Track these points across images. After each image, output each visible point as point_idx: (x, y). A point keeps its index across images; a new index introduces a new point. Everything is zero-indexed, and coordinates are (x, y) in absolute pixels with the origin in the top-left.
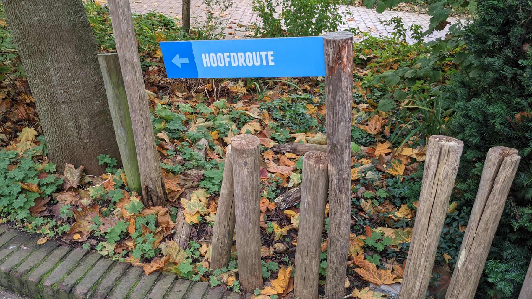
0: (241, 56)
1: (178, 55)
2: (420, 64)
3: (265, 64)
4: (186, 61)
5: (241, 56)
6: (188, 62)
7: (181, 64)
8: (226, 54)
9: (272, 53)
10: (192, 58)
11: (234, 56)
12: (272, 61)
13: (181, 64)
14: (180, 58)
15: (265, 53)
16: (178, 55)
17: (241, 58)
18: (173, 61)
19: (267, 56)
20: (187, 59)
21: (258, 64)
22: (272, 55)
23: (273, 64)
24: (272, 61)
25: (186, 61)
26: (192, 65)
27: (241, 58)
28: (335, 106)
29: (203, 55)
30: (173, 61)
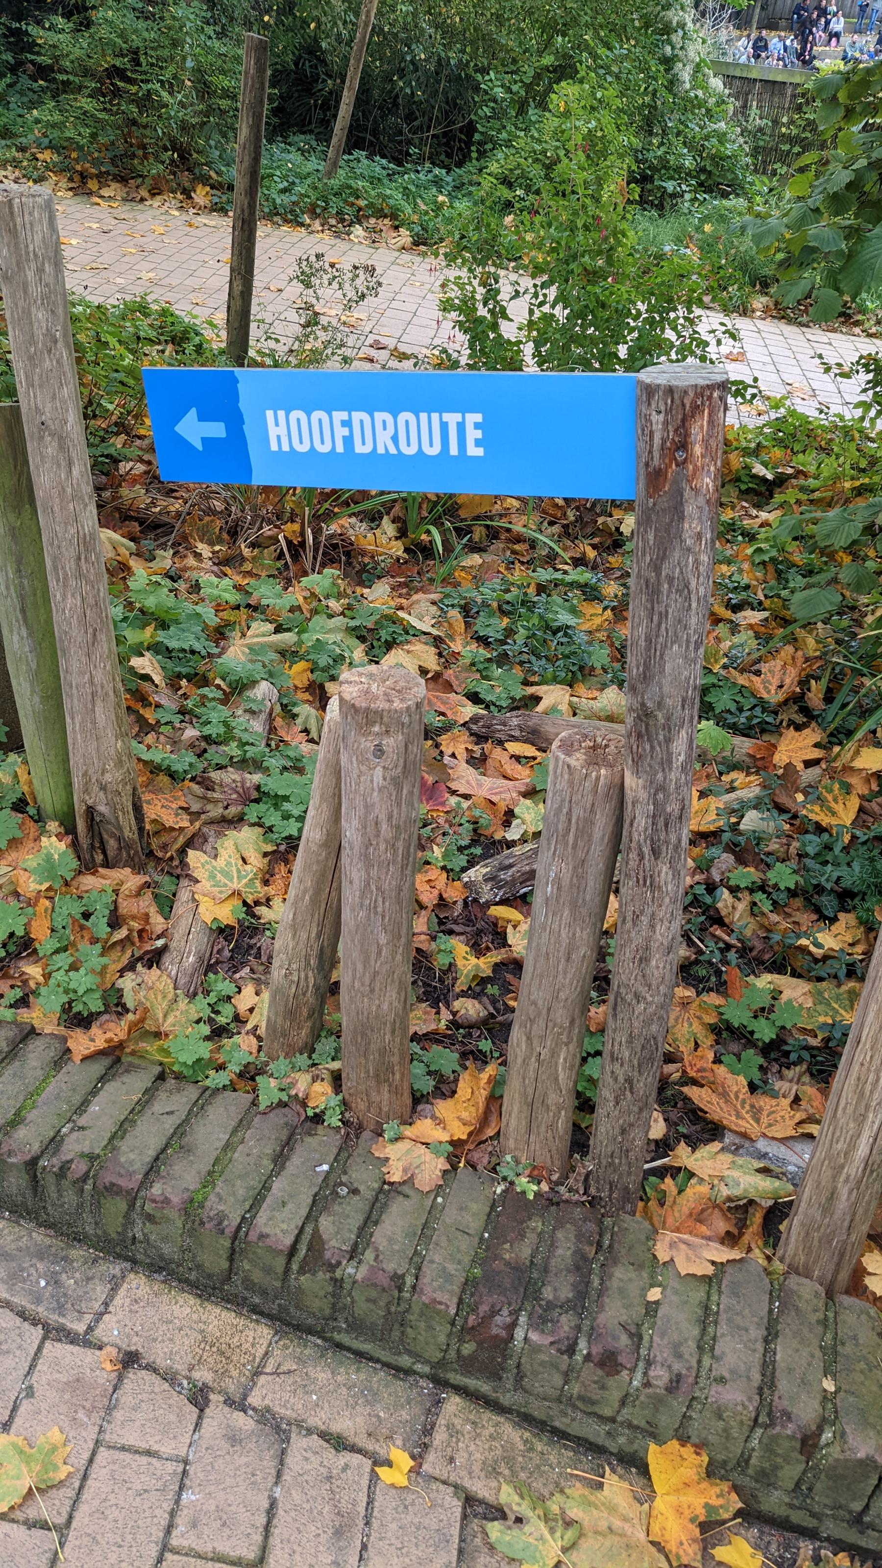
0: (384, 422)
1: (194, 410)
3: (454, 451)
4: (217, 430)
5: (384, 422)
6: (177, 429)
7: (203, 440)
8: (340, 416)
9: (478, 417)
11: (362, 422)
12: (478, 443)
13: (203, 440)
14: (200, 419)
15: (458, 417)
16: (194, 410)
17: (385, 428)
18: (179, 428)
19: (461, 427)
20: (222, 425)
22: (477, 426)
23: (480, 452)
24: (478, 443)
25: (217, 430)
27: (385, 428)
29: (270, 414)
30: (179, 428)
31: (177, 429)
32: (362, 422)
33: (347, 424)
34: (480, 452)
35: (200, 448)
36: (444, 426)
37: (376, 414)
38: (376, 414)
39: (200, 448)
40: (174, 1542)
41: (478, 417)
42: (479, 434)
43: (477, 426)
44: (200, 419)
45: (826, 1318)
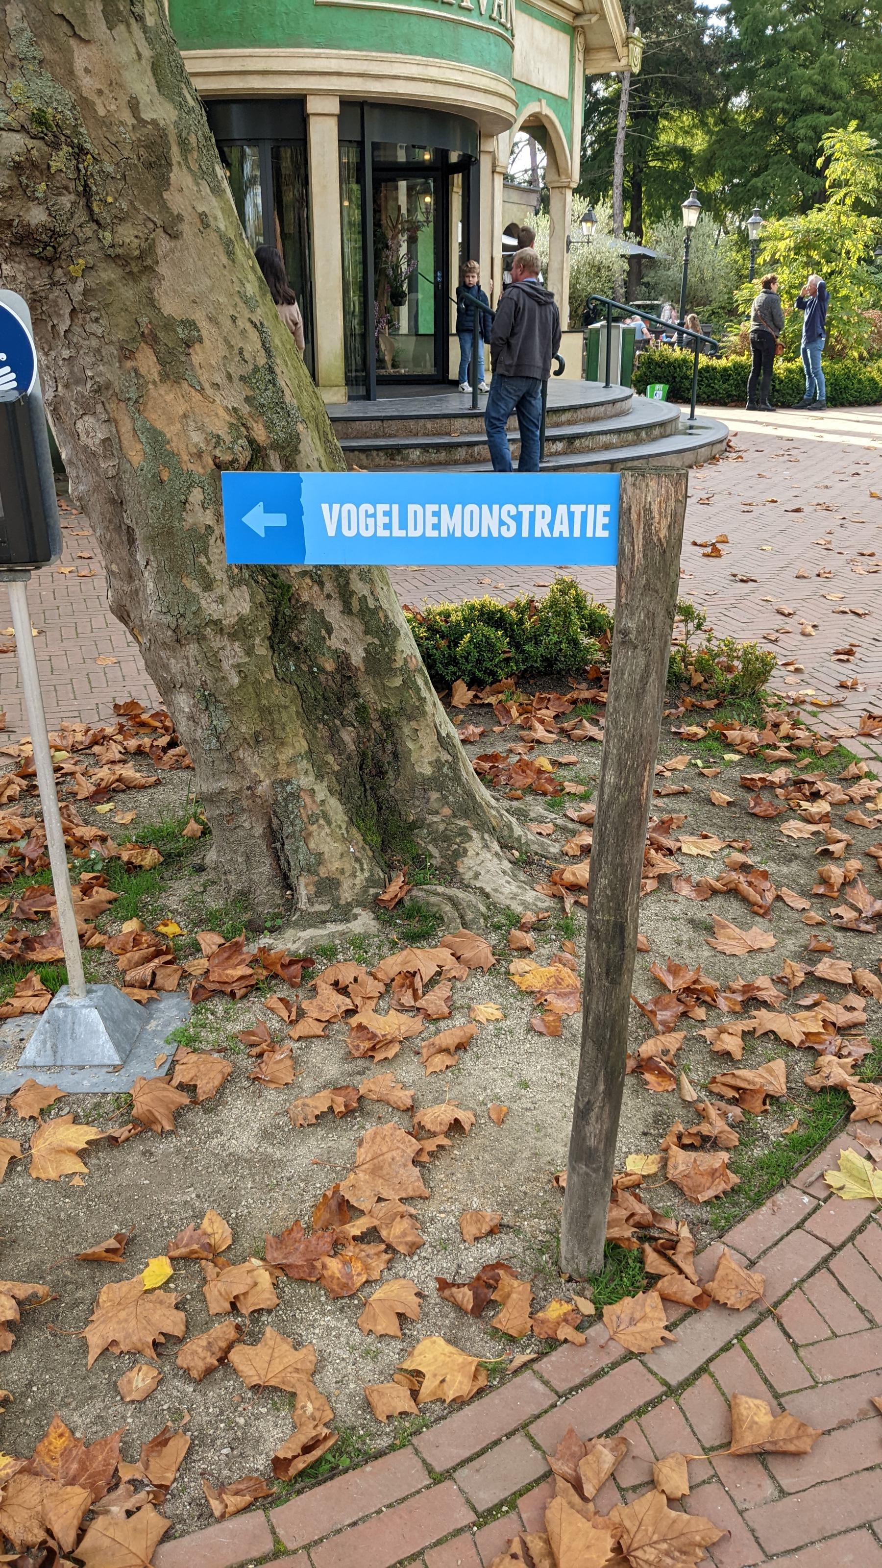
0: (543, 512)
1: (261, 504)
2: (663, 533)
3: (525, 533)
4: (280, 520)
5: (543, 512)
6: (243, 519)
7: (267, 529)
8: (431, 508)
9: (607, 508)
10: (295, 513)
11: (415, 512)
12: (605, 527)
13: (267, 529)
14: (266, 511)
15: (530, 508)
16: (261, 504)
17: (543, 517)
18: (247, 519)
19: (532, 515)
20: (284, 516)
21: (512, 533)
22: (605, 514)
23: (606, 534)
24: (605, 527)
25: (280, 520)
26: (295, 527)
27: (543, 517)
28: (477, 806)
29: (325, 507)
30: (247, 519)
31: (243, 519)
32: (415, 512)
33: (437, 514)
34: (606, 534)
35: (263, 535)
36: (571, 515)
37: (427, 506)
38: (427, 506)
39: (263, 535)
40: (830, 1250)
41: (607, 508)
42: (606, 520)
43: (605, 514)
44: (266, 511)
45: (287, 1462)
